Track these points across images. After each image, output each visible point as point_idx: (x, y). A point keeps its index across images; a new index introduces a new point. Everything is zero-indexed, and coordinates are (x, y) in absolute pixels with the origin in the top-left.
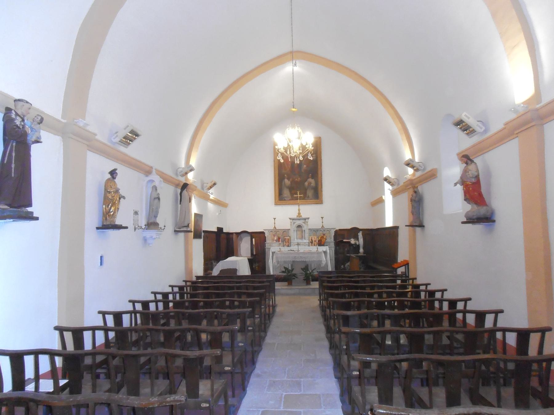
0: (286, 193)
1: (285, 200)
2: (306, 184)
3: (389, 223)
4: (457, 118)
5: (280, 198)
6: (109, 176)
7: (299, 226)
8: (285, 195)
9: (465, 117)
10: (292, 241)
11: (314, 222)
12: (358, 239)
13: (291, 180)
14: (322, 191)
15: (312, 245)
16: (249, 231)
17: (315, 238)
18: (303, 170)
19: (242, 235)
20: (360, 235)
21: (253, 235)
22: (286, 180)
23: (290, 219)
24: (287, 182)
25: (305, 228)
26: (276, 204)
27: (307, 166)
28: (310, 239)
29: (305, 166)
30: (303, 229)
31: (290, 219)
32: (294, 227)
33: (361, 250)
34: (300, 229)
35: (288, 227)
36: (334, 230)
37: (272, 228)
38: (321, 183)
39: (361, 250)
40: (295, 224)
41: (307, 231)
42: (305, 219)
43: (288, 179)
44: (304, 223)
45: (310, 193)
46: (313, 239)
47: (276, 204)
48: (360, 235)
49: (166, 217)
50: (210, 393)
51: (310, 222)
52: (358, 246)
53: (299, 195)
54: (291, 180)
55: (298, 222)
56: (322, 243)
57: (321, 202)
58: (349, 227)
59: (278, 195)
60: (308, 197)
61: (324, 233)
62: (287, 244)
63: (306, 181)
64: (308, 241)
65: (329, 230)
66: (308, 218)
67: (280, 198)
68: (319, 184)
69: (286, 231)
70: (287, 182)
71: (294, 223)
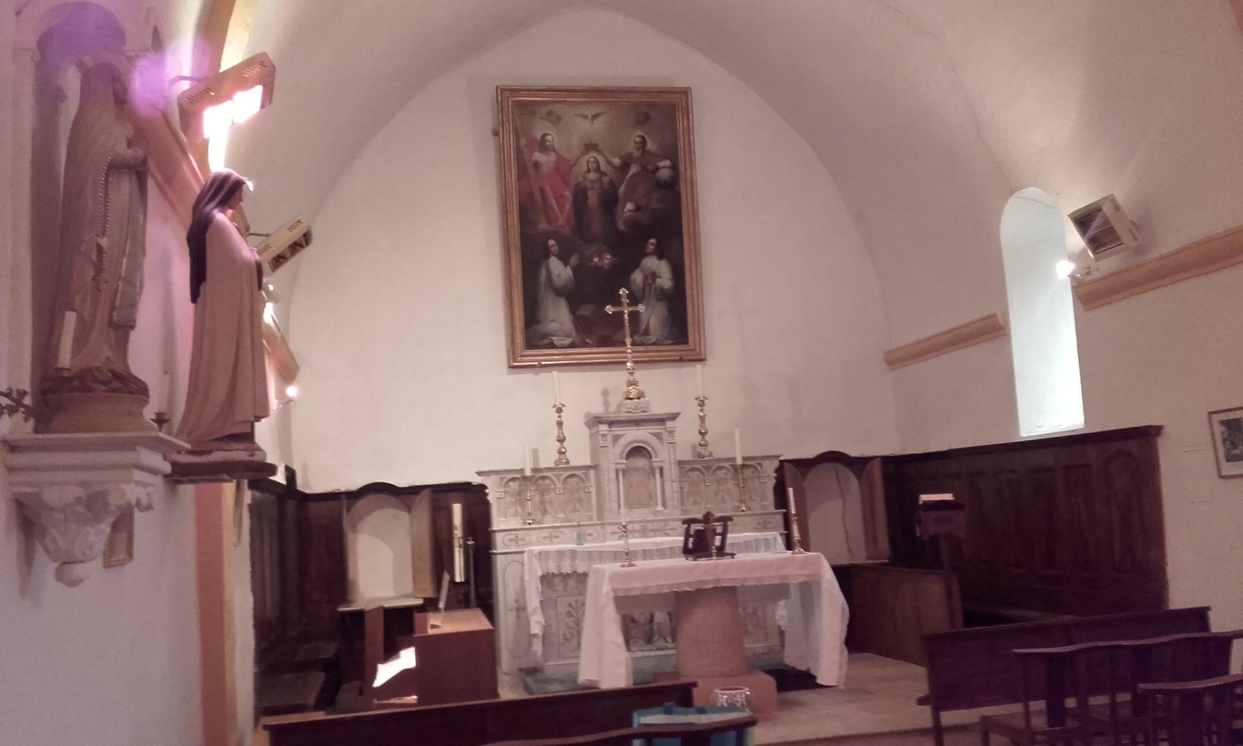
0: (558, 317)
1: (552, 346)
3: (1051, 397)
4: (315, 235)
7: (637, 451)
8: (553, 326)
9: (294, 232)
13: (574, 260)
19: (361, 504)
25: (664, 456)
29: (630, 206)
32: (613, 457)
34: (640, 462)
40: (623, 441)
41: (672, 472)
42: (661, 420)
44: (659, 436)
45: (653, 315)
49: (596, 225)
54: (574, 260)
55: (633, 435)
63: (636, 264)
70: (560, 271)
71: (616, 438)
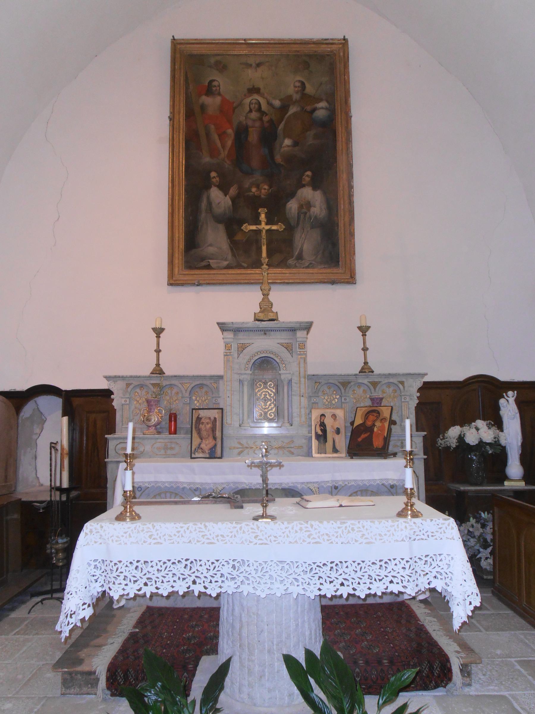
0: (215, 239)
1: (208, 267)
2: (292, 206)
5: (192, 257)
6: (404, 506)
7: (264, 363)
8: (211, 250)
10: (228, 431)
11: (331, 351)
12: (497, 422)
13: (233, 191)
14: (352, 235)
15: (322, 450)
16: (64, 387)
17: (339, 418)
18: (278, 159)
20: (509, 408)
21: (76, 401)
22: (215, 194)
23: (223, 327)
24: (219, 199)
25: (289, 370)
26: (174, 281)
27: (296, 144)
28: (315, 414)
29: (287, 142)
30: (285, 375)
31: (223, 327)
33: (515, 468)
35: (214, 365)
36: (419, 384)
37: (145, 369)
38: (351, 203)
39: (515, 468)
42: (293, 330)
43: (224, 188)
44: (289, 348)
45: (306, 242)
46: (328, 421)
47: (174, 281)
48: (509, 408)
50: (298, 379)
51: (313, 341)
52: (496, 457)
53: (264, 227)
54: (233, 191)
56: (378, 443)
57: (350, 278)
58: (458, 374)
59: (181, 245)
60: (300, 257)
61: (378, 394)
62: (207, 445)
63: (292, 195)
64: (304, 431)
65: (398, 381)
66: (307, 327)
67: (192, 257)
68: (342, 206)
69: (205, 385)
71: (242, 348)
